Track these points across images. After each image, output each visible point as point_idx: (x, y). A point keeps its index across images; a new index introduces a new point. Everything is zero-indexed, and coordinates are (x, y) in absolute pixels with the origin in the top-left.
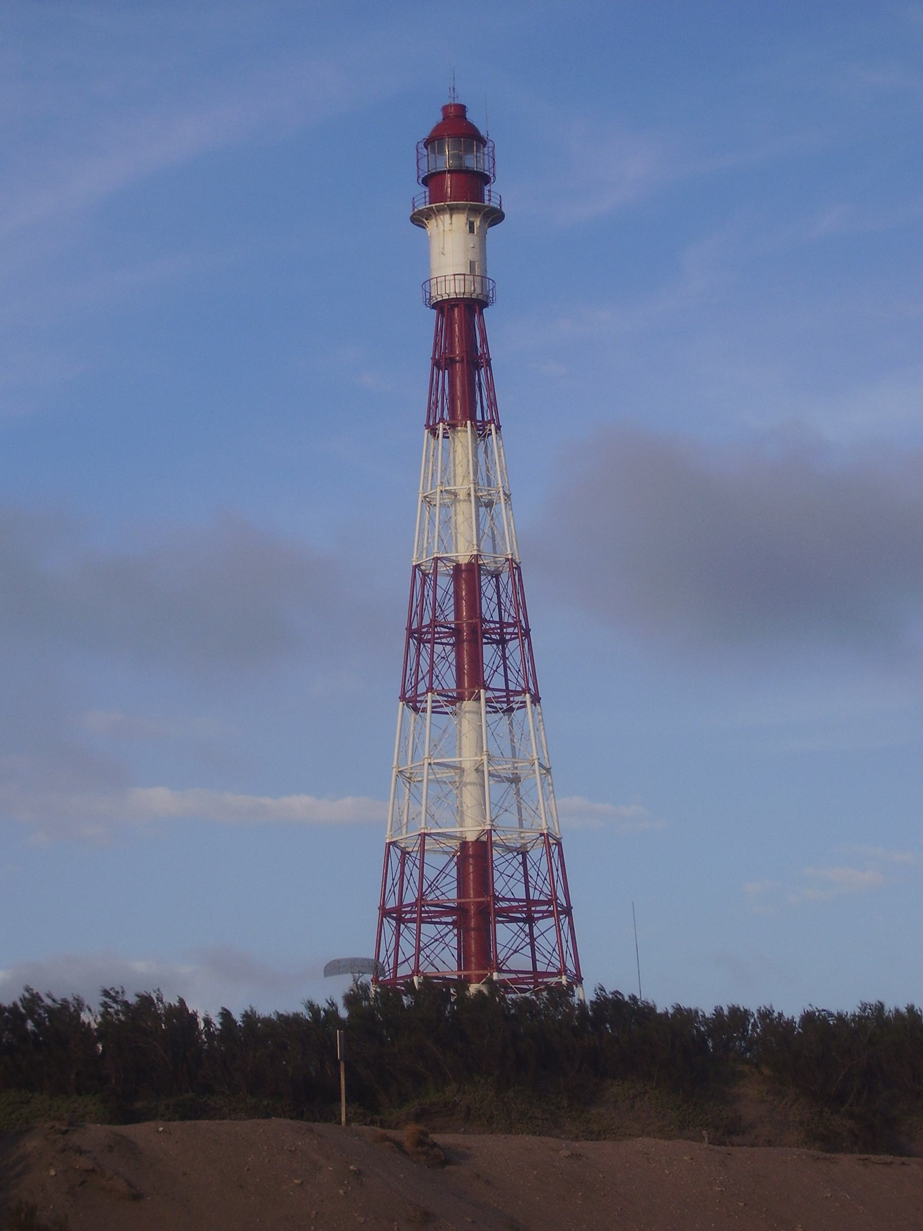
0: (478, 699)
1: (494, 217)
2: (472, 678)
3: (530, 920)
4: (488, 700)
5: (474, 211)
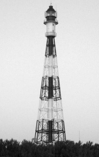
0: (52, 98)
1: (57, 23)
2: (51, 96)
3: (58, 133)
4: (54, 99)
5: (54, 22)
